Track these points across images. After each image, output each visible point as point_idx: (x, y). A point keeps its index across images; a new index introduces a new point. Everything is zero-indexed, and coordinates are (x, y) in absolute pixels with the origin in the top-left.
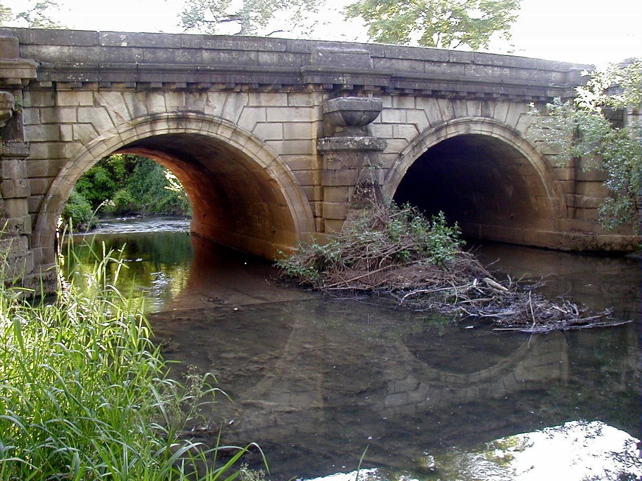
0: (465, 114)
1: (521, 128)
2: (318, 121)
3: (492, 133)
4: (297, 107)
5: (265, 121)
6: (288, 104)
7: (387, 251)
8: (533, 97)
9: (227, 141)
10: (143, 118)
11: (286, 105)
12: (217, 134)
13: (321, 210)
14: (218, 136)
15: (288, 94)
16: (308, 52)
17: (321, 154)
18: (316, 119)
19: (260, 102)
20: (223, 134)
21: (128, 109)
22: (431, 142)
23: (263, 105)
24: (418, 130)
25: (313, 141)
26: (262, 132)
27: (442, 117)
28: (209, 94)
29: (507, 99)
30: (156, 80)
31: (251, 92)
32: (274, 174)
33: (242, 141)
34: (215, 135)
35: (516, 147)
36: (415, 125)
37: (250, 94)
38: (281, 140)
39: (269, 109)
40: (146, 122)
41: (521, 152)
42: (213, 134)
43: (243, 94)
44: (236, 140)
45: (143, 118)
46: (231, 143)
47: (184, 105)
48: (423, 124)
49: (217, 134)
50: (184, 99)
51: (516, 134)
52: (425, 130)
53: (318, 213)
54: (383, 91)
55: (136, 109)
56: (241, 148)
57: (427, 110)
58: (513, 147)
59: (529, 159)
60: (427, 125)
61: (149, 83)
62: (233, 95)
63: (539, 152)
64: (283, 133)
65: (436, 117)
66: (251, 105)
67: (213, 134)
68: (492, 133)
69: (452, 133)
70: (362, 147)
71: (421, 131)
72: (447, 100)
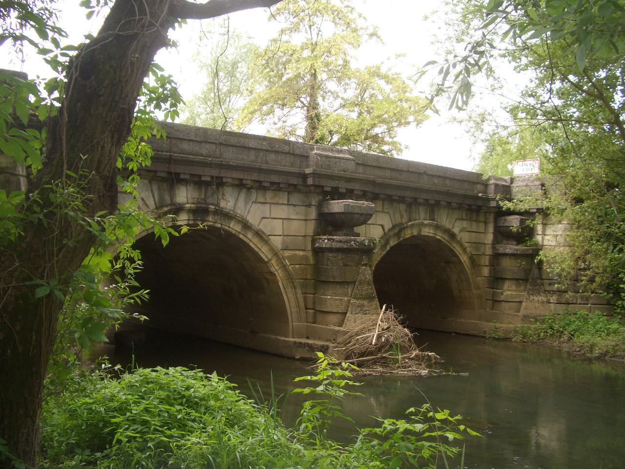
0: (417, 217)
1: (456, 230)
2: (314, 220)
3: (436, 234)
4: (295, 205)
5: (268, 216)
6: (288, 201)
7: (350, 342)
8: (192, 175)
9: (237, 234)
10: (169, 208)
11: (286, 203)
12: (229, 227)
13: (314, 303)
14: (230, 229)
15: (289, 193)
16: (306, 154)
17: (318, 252)
18: (314, 218)
19: (266, 199)
20: (234, 227)
21: (154, 197)
22: (393, 242)
23: (268, 201)
24: (384, 230)
25: (308, 238)
26: (265, 227)
27: (401, 219)
28: (225, 188)
29: (240, 185)
30: (184, 171)
31: (260, 189)
32: (275, 267)
33: (250, 235)
34: (228, 228)
35: (452, 247)
36: (382, 226)
37: (386, 203)
38: (281, 236)
39: (272, 206)
40: (169, 212)
41: (456, 251)
42: (226, 227)
43: (252, 190)
44: (245, 234)
45: (169, 208)
46: (241, 236)
47: (203, 197)
48: (388, 226)
49: (229, 227)
50: (203, 192)
51: (453, 236)
52: (389, 230)
53: (310, 305)
54: (374, 198)
55: (161, 198)
56: (248, 241)
57: (391, 213)
58: (449, 247)
59: (461, 258)
60: (391, 226)
61: (200, 176)
62: (244, 191)
63: (468, 252)
64: (283, 229)
65: (398, 220)
66: (258, 201)
67: (226, 227)
68: (436, 234)
69: (408, 234)
70: (362, 247)
71: (386, 230)
72: (405, 205)
